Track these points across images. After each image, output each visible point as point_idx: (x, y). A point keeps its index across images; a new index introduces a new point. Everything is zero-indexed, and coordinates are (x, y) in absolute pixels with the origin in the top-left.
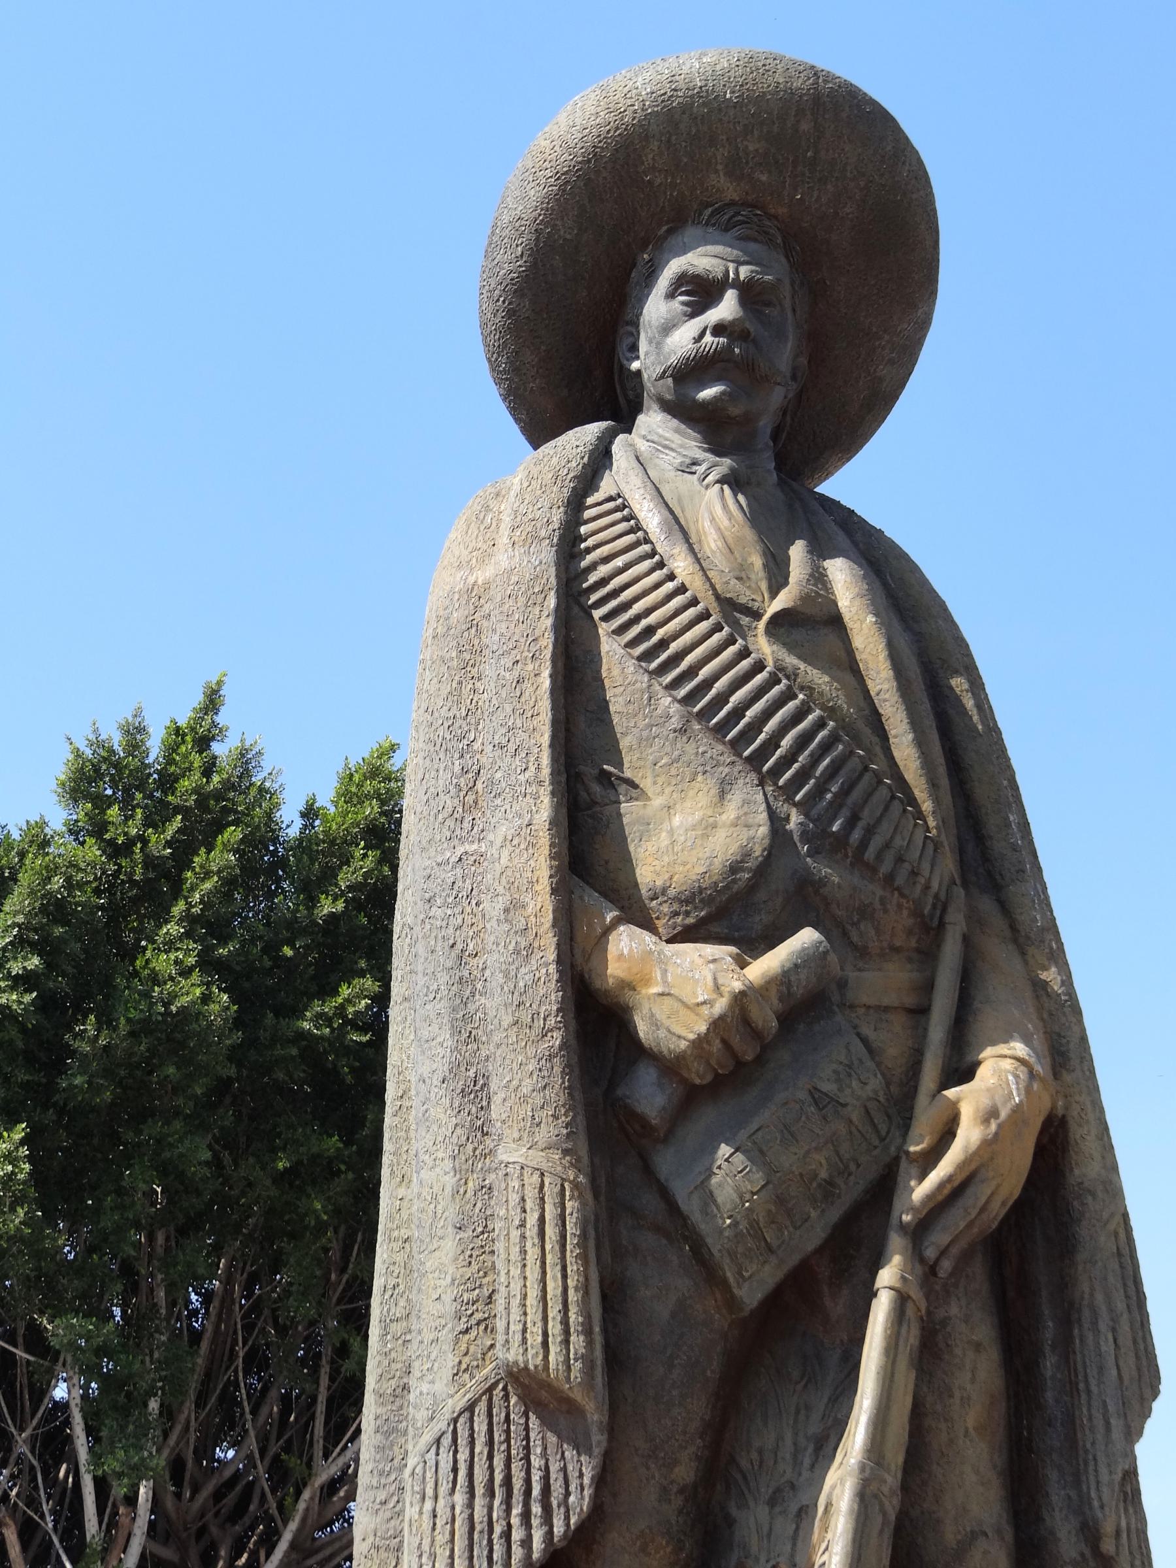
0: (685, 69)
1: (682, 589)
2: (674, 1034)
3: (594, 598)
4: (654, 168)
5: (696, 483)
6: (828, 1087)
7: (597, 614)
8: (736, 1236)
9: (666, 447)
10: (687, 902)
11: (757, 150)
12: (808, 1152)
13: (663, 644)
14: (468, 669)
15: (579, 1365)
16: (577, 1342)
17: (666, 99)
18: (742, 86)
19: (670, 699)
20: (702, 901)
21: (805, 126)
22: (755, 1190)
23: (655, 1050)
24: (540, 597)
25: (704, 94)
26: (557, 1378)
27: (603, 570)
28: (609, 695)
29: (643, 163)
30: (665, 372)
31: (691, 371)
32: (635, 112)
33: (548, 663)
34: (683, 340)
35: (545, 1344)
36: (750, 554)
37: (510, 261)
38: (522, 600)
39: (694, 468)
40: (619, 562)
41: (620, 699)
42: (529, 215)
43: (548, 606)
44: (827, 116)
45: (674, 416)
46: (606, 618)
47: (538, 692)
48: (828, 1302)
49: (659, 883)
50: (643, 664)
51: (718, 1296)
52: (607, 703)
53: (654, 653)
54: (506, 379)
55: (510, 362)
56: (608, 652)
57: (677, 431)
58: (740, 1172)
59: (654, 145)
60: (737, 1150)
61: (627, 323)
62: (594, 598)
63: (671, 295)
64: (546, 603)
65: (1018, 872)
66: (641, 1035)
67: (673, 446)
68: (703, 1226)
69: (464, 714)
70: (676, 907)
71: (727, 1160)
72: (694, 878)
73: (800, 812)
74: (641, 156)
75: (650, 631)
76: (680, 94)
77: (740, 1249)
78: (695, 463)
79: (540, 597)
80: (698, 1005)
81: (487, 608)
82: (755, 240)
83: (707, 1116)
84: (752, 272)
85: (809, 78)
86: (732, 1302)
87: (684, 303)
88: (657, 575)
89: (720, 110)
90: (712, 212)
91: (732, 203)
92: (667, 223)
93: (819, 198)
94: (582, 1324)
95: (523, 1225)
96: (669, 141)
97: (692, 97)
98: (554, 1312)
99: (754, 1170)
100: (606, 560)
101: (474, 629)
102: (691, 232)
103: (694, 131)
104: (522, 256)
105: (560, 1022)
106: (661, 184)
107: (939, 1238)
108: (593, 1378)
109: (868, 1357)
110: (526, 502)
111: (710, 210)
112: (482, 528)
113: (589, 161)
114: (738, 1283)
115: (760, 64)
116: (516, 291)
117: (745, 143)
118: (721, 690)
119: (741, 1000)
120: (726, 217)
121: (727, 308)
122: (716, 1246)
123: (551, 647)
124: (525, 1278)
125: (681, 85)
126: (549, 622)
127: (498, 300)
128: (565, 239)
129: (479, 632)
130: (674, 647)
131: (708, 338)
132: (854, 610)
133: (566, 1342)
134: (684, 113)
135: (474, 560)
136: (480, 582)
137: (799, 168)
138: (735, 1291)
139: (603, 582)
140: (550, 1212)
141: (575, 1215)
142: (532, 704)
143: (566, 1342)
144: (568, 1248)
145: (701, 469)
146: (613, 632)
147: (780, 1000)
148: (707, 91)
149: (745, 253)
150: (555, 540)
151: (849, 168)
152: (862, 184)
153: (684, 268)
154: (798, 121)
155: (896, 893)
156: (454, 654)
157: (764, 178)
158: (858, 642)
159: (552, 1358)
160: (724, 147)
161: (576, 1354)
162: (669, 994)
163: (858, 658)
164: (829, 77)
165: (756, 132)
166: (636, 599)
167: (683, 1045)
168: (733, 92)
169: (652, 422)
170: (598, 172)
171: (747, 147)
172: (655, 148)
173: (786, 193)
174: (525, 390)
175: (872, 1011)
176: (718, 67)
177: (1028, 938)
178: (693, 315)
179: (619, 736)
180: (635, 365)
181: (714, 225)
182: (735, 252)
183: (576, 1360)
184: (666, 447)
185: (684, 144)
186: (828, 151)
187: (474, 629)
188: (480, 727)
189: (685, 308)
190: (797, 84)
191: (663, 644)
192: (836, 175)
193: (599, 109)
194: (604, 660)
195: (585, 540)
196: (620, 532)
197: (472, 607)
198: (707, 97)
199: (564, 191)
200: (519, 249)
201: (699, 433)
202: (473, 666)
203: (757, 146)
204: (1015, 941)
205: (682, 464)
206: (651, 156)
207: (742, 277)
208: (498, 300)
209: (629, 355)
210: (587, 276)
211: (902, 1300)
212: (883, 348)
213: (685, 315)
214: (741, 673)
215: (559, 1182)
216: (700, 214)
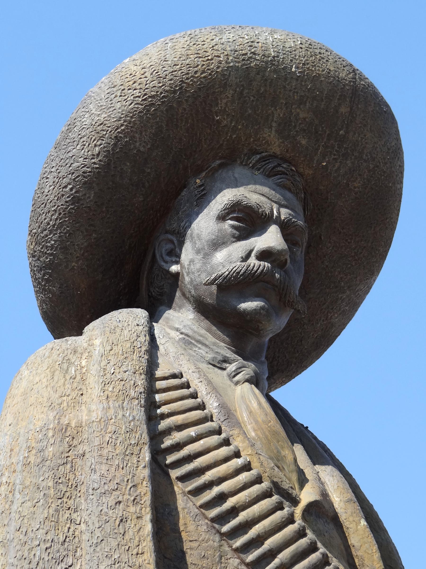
0: (262, 39)
1: (247, 467)
3: (170, 459)
5: (226, 378)
7: (174, 474)
9: (199, 342)
11: (305, 119)
13: (234, 511)
14: (65, 500)
17: (247, 59)
18: (304, 64)
19: (237, 561)
21: (344, 110)
24: (136, 450)
25: (276, 63)
27: (177, 437)
28: (186, 546)
29: (217, 105)
30: (215, 279)
31: (235, 285)
32: (220, 62)
33: (148, 509)
34: (229, 259)
36: (282, 448)
37: (84, 155)
38: (120, 449)
39: (225, 365)
40: (192, 432)
41: (195, 552)
42: (112, 122)
43: (144, 458)
44: (360, 106)
45: (207, 318)
46: (183, 479)
47: (141, 533)
50: (217, 526)
52: (184, 554)
53: (224, 519)
54: (51, 254)
55: (61, 240)
56: (183, 509)
57: (209, 330)
59: (230, 93)
61: (173, 233)
62: (170, 459)
63: (222, 218)
64: (142, 456)
67: (207, 343)
69: (62, 539)
74: (217, 99)
75: (222, 498)
76: (258, 58)
78: (226, 360)
79: (136, 450)
81: (81, 449)
82: (289, 190)
84: (290, 214)
85: (350, 73)
88: (224, 451)
89: (286, 79)
90: (260, 159)
91: (274, 156)
92: (220, 158)
93: (339, 168)
96: (241, 93)
97: (266, 62)
100: (180, 428)
101: (69, 466)
102: (239, 171)
103: (262, 89)
104: (98, 155)
106: (226, 126)
110: (112, 363)
111: (258, 156)
112: (68, 377)
113: (175, 92)
115: (317, 51)
116: (85, 183)
117: (298, 110)
118: (285, 561)
120: (271, 165)
121: (271, 238)
123: (149, 494)
125: (259, 51)
126: (146, 472)
127: (66, 187)
128: (139, 151)
129: (73, 469)
130: (243, 516)
131: (253, 261)
132: (349, 511)
134: (258, 74)
135: (65, 404)
136: (73, 425)
139: (178, 447)
142: (136, 542)
145: (231, 368)
146: (190, 492)
148: (278, 62)
149: (285, 199)
150: (143, 402)
151: (365, 152)
152: (371, 166)
153: (240, 198)
154: (340, 104)
156: (51, 484)
157: (304, 142)
158: (354, 540)
160: (281, 108)
163: (354, 553)
164: (362, 78)
166: (209, 467)
168: (297, 68)
169: (180, 319)
170: (180, 103)
171: (298, 114)
172: (230, 96)
173: (316, 158)
174: (66, 267)
176: (287, 45)
178: (239, 238)
180: (174, 268)
181: (259, 169)
182: (278, 196)
184: (199, 342)
185: (252, 98)
186: (355, 134)
187: (69, 466)
188: (78, 554)
189: (235, 232)
190: (342, 75)
191: (234, 511)
192: (356, 154)
193: (189, 52)
194: (181, 516)
195: (159, 407)
196: (190, 406)
197: (67, 446)
198: (278, 66)
199: (148, 111)
200: (97, 149)
201: (228, 336)
202: (69, 498)
205: (214, 359)
206: (224, 101)
207: (283, 217)
208: (66, 187)
209: (168, 258)
210: (147, 185)
213: (233, 236)
214: (300, 549)
216: (249, 158)
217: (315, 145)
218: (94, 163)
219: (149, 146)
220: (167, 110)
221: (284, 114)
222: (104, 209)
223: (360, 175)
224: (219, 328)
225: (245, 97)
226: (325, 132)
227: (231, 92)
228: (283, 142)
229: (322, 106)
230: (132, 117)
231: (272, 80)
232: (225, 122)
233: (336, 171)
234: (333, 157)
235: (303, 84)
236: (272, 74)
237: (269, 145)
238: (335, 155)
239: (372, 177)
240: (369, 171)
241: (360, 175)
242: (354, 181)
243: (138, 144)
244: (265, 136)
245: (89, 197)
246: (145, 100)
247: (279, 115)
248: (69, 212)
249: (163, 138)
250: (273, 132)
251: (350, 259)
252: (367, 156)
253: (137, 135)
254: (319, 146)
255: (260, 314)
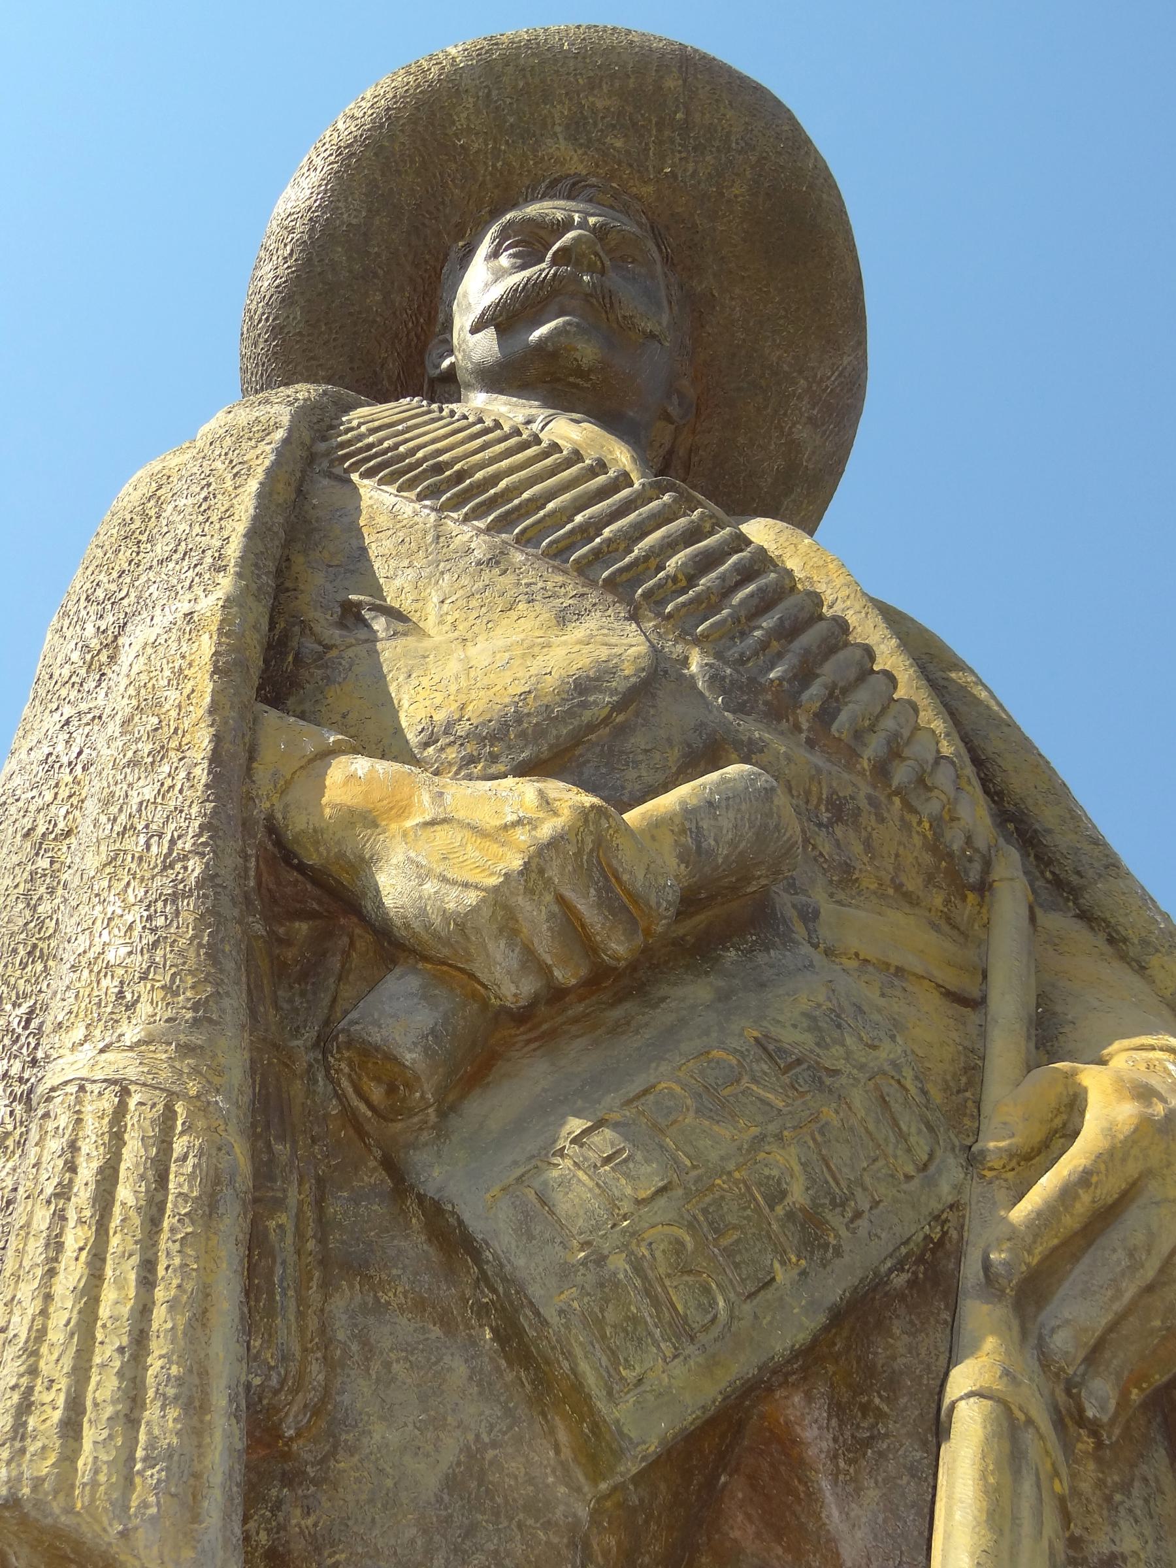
2: (454, 883)
4: (469, 130)
6: (795, 1038)
8: (602, 1285)
10: (493, 738)
11: (607, 109)
12: (760, 1139)
15: (154, 1474)
16: (160, 1421)
20: (522, 735)
21: (670, 83)
22: (643, 1194)
23: (416, 925)
26: (90, 1507)
29: (453, 123)
35: (71, 1427)
48: (833, 1515)
49: (440, 717)
51: (563, 1436)
58: (607, 1160)
60: (600, 1124)
65: (1107, 867)
66: (388, 902)
68: (521, 1262)
70: (470, 748)
71: (574, 1141)
72: (507, 700)
73: (703, 652)
74: (451, 116)
77: (612, 1315)
80: (505, 827)
83: (530, 1077)
86: (596, 1447)
87: (514, 256)
89: (556, 61)
93: (695, 172)
94: (180, 1381)
95: (64, 1192)
96: (488, 95)
98: (108, 1350)
99: (639, 1156)
103: (521, 84)
104: (291, 254)
105: (204, 844)
106: (478, 151)
107: (1076, 1316)
108: (196, 1518)
109: (950, 1497)
113: (382, 126)
114: (610, 1394)
117: (591, 99)
119: (597, 823)
122: (555, 1301)
124: (48, 1297)
133: (130, 1418)
137: (667, 133)
138: (601, 1405)
140: (133, 1152)
141: (191, 1161)
143: (130, 1418)
144: (166, 1224)
147: (683, 858)
151: (733, 138)
152: (753, 159)
154: (662, 77)
155: (897, 800)
157: (619, 144)
159: (84, 1462)
161: (151, 1445)
162: (445, 821)
165: (604, 86)
167: (472, 898)
168: (571, 44)
171: (593, 103)
172: (471, 106)
175: (871, 969)
177: (1144, 942)
179: (381, 581)
183: (149, 1461)
185: (508, 101)
186: (703, 114)
192: (717, 144)
200: (288, 248)
203: (608, 103)
204: (1123, 957)
206: (465, 115)
210: (380, 272)
211: (1009, 1429)
212: (800, 398)
215: (161, 1100)
217: (640, 143)
218: (288, 267)
219: (364, 214)
220: (376, 154)
221: (570, 109)
222: (323, 328)
223: (737, 175)
224: (519, 397)
225: (496, 102)
226: (650, 121)
227: (471, 100)
228: (585, 153)
229: (632, 86)
230: (326, 185)
231: (533, 67)
232: (476, 145)
233: (693, 176)
234: (678, 155)
235: (588, 61)
236: (531, 59)
237: (563, 164)
238: (680, 152)
239: (760, 176)
240: (752, 167)
241: (737, 175)
242: (732, 186)
243: (345, 216)
244: (550, 151)
245: (294, 318)
246: (340, 154)
247: (562, 113)
248: (274, 353)
249: (382, 195)
250: (561, 140)
251: (781, 322)
252: (737, 144)
253: (340, 204)
254: (647, 144)
255: (567, 332)
